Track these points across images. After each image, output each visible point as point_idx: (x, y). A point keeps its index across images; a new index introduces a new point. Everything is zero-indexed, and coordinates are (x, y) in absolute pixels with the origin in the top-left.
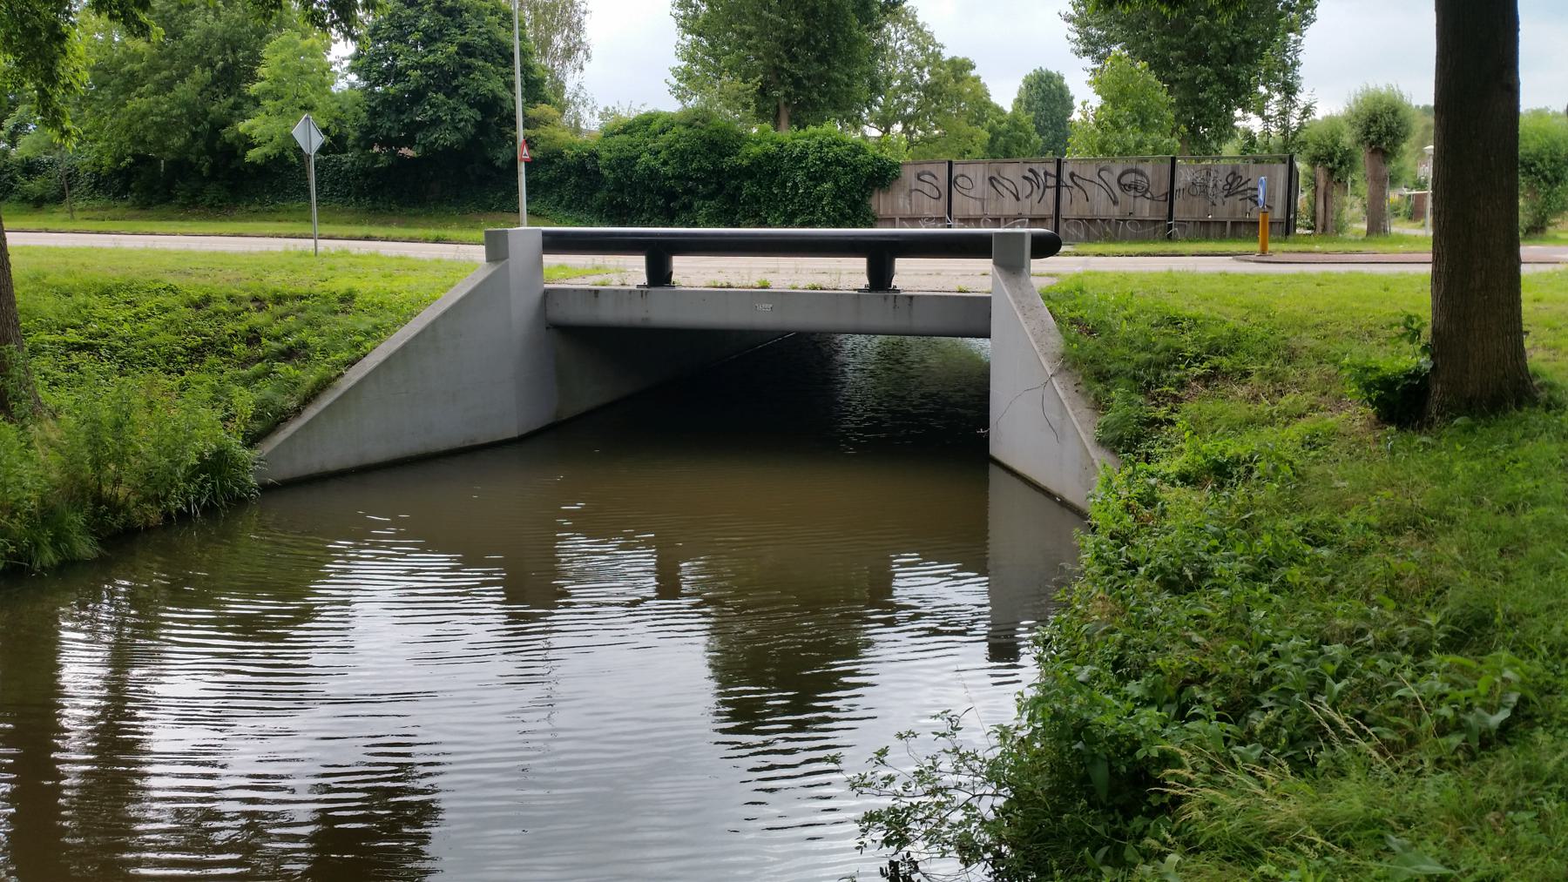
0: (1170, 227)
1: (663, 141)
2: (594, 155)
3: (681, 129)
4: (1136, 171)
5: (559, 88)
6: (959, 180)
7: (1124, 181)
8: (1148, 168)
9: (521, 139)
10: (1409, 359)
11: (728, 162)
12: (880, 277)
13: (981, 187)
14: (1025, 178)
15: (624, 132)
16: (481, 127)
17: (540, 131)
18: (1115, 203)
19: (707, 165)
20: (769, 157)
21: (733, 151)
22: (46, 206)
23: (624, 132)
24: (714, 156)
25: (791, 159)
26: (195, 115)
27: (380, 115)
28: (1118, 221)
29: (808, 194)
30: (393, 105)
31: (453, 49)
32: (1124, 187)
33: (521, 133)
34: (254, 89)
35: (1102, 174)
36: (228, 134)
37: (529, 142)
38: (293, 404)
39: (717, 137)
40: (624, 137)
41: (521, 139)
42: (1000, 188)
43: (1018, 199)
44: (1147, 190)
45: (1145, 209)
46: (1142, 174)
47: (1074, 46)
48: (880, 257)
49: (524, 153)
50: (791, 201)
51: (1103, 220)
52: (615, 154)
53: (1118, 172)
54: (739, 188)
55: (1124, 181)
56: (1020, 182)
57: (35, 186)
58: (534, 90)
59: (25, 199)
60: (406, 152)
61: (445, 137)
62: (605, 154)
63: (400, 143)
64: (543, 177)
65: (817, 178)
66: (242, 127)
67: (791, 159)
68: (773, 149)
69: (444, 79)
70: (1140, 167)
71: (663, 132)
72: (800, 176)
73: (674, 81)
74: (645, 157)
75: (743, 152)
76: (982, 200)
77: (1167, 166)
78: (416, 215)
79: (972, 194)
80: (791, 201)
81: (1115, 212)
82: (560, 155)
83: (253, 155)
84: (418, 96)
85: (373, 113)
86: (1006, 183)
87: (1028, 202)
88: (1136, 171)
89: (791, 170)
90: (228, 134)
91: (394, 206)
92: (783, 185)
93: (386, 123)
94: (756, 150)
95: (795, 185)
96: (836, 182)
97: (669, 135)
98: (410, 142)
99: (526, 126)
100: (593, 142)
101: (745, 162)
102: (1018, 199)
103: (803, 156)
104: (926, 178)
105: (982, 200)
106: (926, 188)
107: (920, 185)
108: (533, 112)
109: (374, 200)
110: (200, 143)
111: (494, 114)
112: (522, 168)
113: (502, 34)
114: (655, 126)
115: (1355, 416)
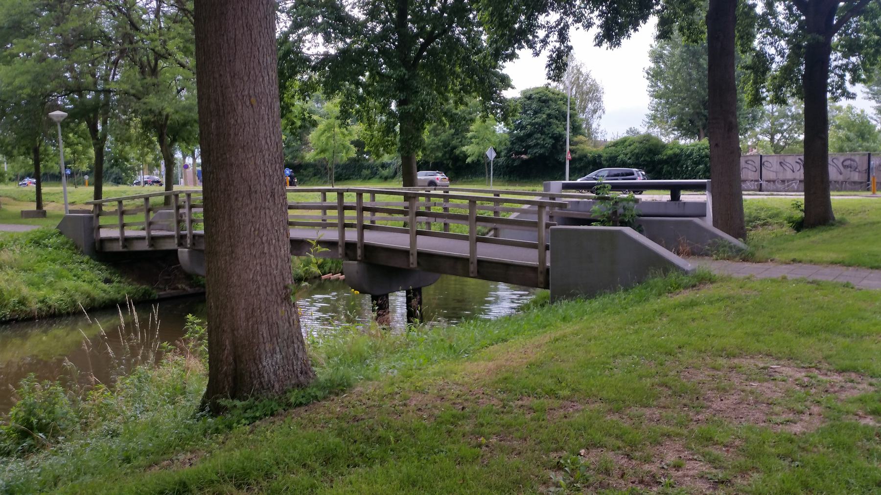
0: (868, 185)
1: (629, 149)
2: (600, 156)
3: (637, 144)
4: (851, 160)
5: (589, 126)
6: (765, 163)
7: (845, 163)
8: (857, 158)
9: (568, 150)
10: (799, 215)
11: (657, 157)
12: (675, 197)
13: (776, 166)
14: (797, 162)
15: (614, 146)
16: (554, 146)
17: (578, 147)
18: (841, 174)
19: (647, 159)
20: (676, 155)
21: (659, 153)
22: (389, 180)
23: (614, 146)
24: (651, 155)
25: (686, 155)
26: (446, 144)
27: (515, 143)
28: (842, 182)
29: (692, 170)
30: (520, 139)
31: (544, 116)
32: (845, 167)
33: (568, 147)
34: (469, 135)
35: (834, 160)
36: (457, 152)
37: (572, 151)
38: (487, 231)
39: (653, 148)
40: (613, 148)
41: (568, 150)
42: (785, 167)
43: (793, 172)
44: (856, 168)
45: (856, 177)
46: (854, 161)
47: (865, 95)
48: (675, 191)
49: (569, 156)
50: (685, 173)
51: (835, 182)
52: (609, 155)
53: (842, 159)
54: (662, 168)
55: (845, 163)
56: (794, 164)
57: (385, 172)
58: (576, 129)
59: (381, 177)
60: (524, 157)
61: (538, 151)
62: (605, 155)
63: (522, 153)
64: (578, 165)
65: (697, 163)
66: (464, 149)
67: (686, 155)
68: (678, 151)
69: (540, 128)
70: (853, 157)
71: (630, 146)
72: (689, 162)
73: (647, 120)
74: (621, 156)
75: (664, 153)
76: (776, 172)
77: (866, 157)
78: (526, 182)
79: (772, 169)
80: (685, 173)
81: (841, 178)
82: (585, 156)
83: (469, 160)
84: (529, 135)
85: (513, 143)
86: (788, 165)
87: (798, 173)
88: (851, 160)
89: (686, 160)
90: (457, 152)
91: (518, 179)
92: (682, 167)
93: (516, 147)
94: (670, 152)
95: (687, 167)
96: (706, 165)
97: (632, 147)
98: (525, 153)
99: (570, 145)
100: (600, 150)
101: (665, 157)
102: (793, 172)
103: (691, 154)
104: (750, 162)
105: (776, 172)
106: (750, 167)
107: (747, 166)
108: (575, 139)
109: (510, 177)
110: (447, 156)
111: (559, 139)
112: (568, 162)
113: (564, 108)
114: (627, 143)
115: (787, 230)
